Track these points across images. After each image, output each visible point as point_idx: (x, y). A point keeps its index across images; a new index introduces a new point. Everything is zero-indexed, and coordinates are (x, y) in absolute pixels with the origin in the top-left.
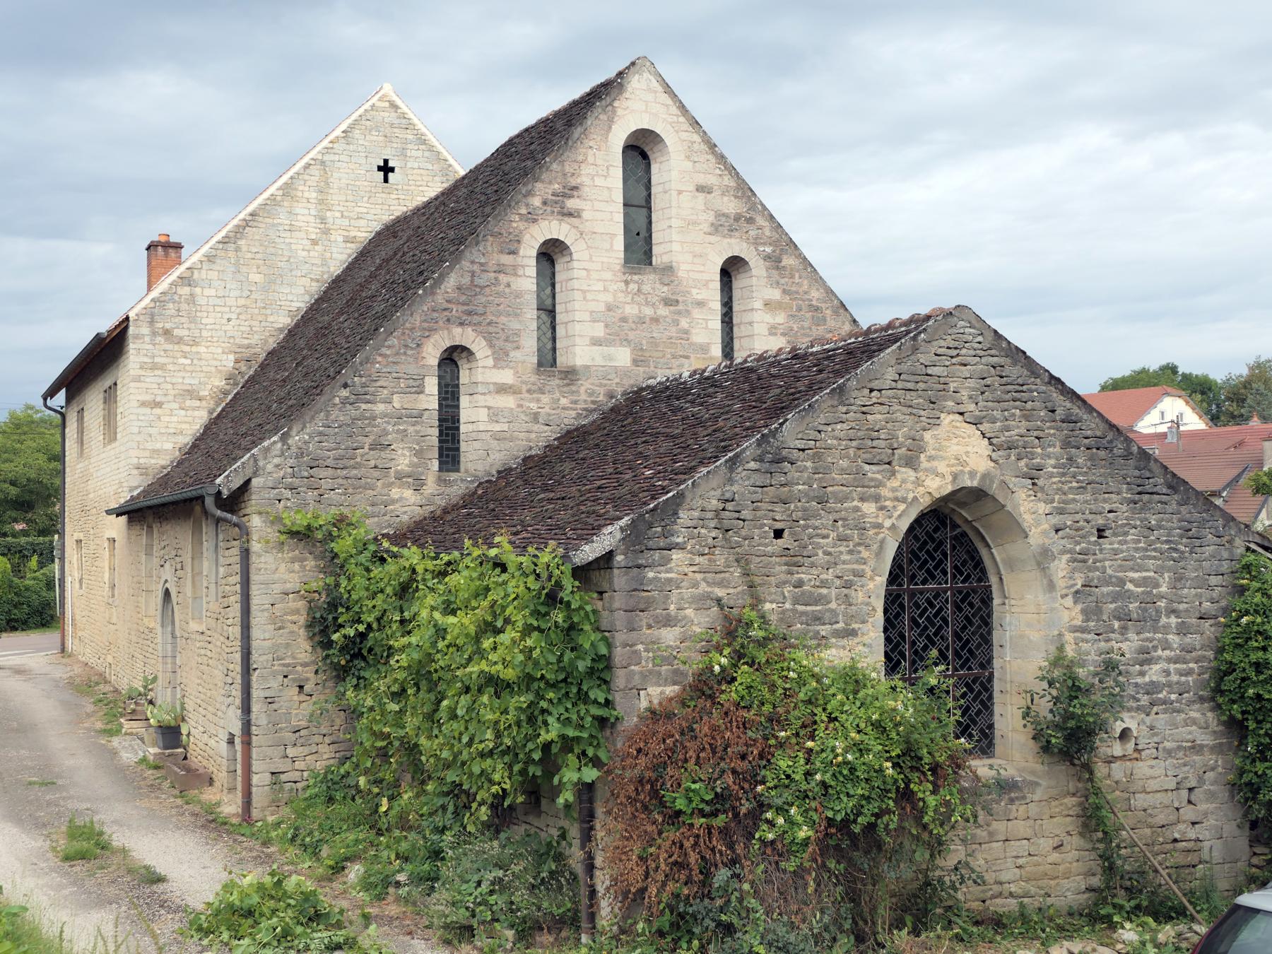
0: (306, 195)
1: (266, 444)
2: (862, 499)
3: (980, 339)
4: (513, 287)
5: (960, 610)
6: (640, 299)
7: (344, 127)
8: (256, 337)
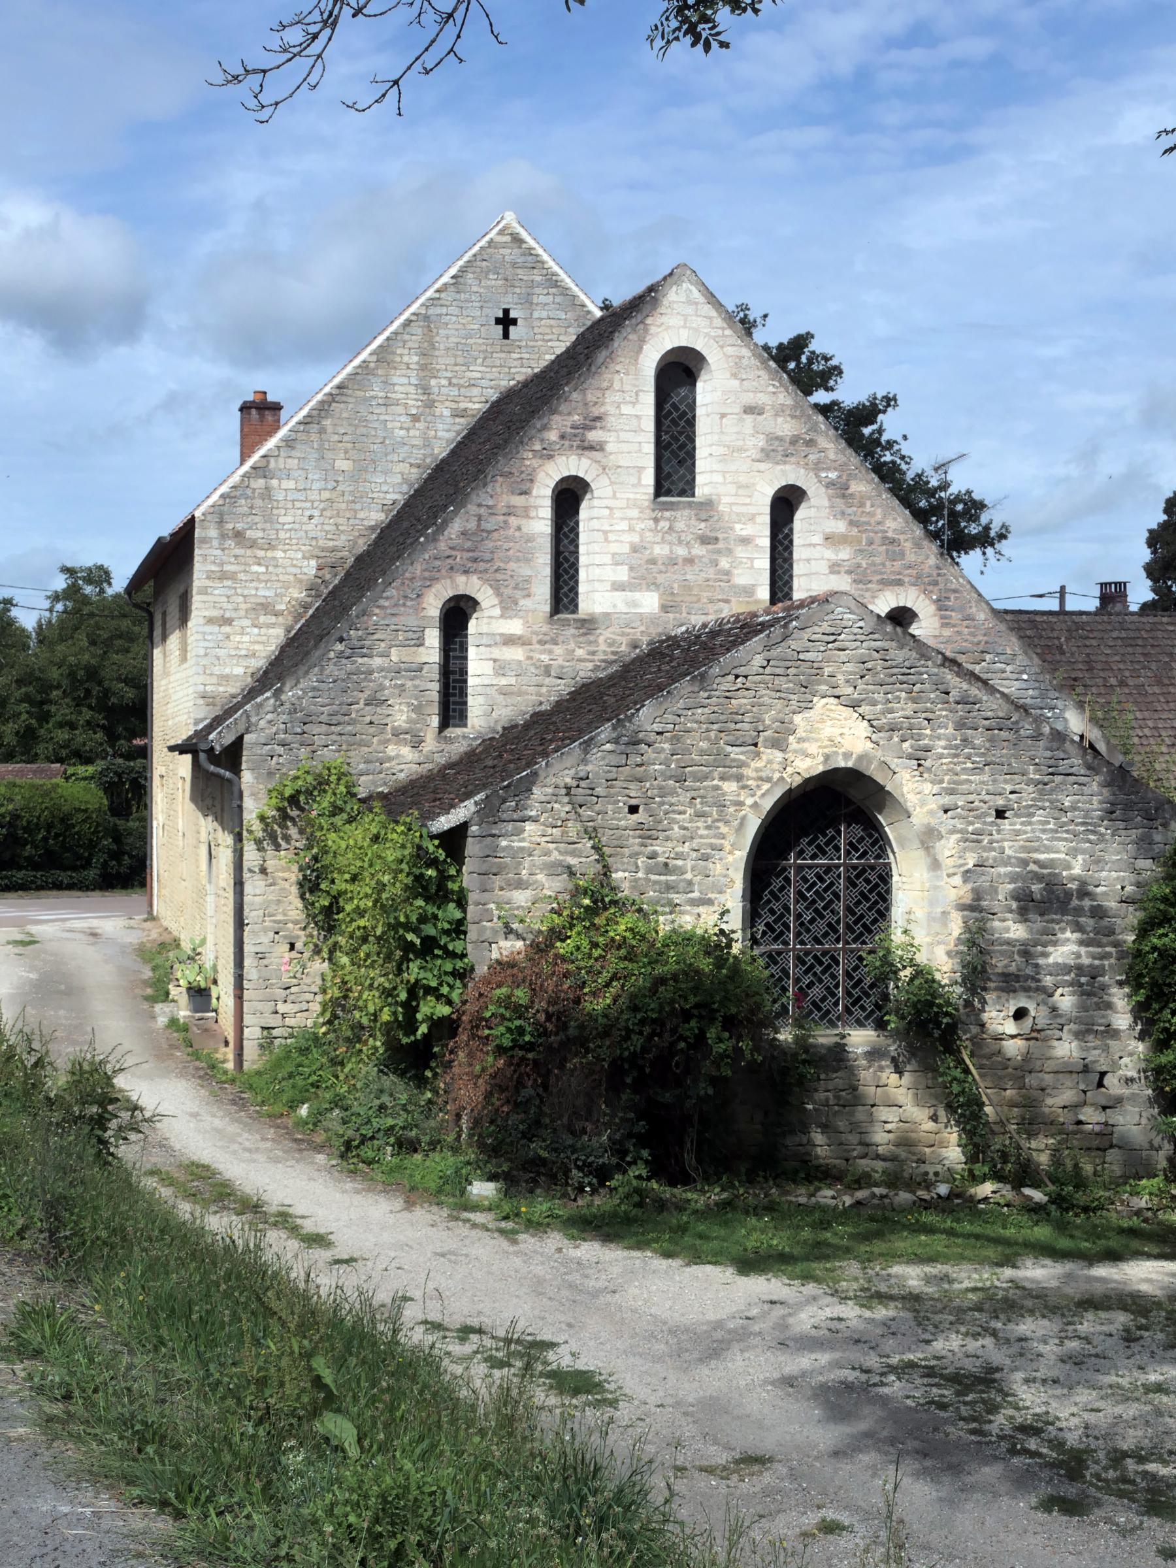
0: (406, 359)
1: (259, 700)
2: (722, 778)
3: (861, 624)
4: (524, 530)
5: (854, 885)
6: (673, 538)
7: (453, 271)
8: (343, 537)
